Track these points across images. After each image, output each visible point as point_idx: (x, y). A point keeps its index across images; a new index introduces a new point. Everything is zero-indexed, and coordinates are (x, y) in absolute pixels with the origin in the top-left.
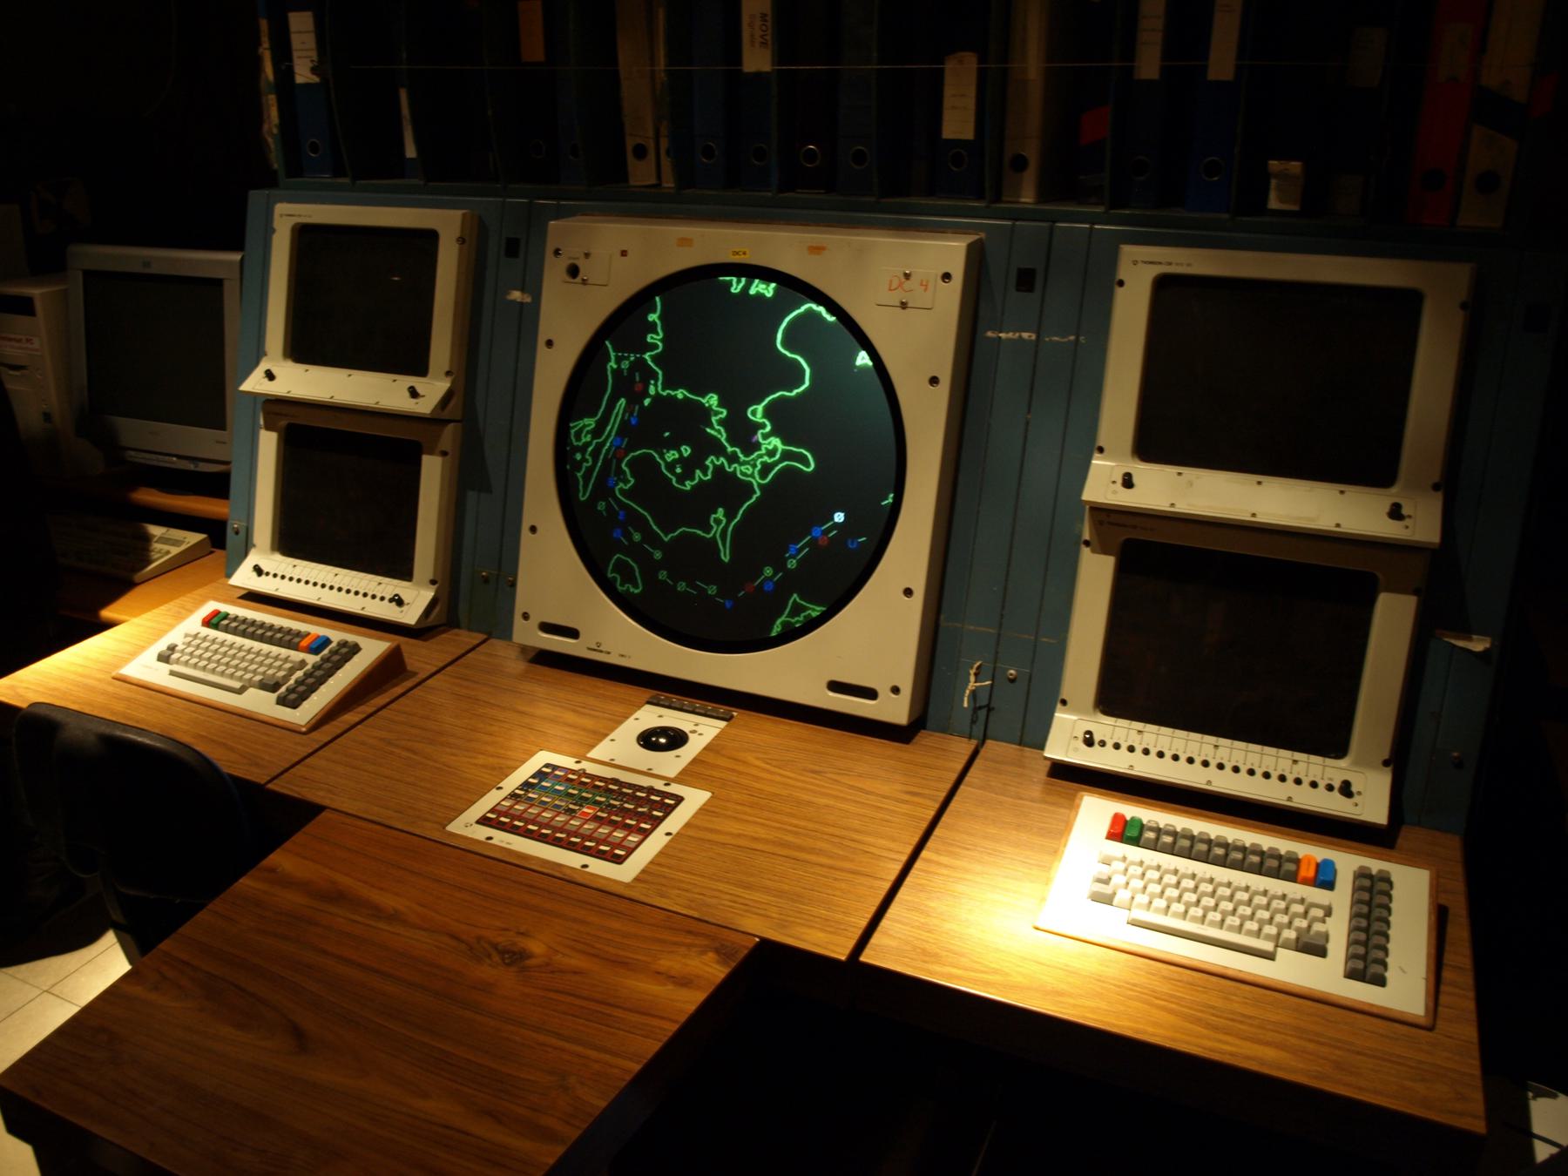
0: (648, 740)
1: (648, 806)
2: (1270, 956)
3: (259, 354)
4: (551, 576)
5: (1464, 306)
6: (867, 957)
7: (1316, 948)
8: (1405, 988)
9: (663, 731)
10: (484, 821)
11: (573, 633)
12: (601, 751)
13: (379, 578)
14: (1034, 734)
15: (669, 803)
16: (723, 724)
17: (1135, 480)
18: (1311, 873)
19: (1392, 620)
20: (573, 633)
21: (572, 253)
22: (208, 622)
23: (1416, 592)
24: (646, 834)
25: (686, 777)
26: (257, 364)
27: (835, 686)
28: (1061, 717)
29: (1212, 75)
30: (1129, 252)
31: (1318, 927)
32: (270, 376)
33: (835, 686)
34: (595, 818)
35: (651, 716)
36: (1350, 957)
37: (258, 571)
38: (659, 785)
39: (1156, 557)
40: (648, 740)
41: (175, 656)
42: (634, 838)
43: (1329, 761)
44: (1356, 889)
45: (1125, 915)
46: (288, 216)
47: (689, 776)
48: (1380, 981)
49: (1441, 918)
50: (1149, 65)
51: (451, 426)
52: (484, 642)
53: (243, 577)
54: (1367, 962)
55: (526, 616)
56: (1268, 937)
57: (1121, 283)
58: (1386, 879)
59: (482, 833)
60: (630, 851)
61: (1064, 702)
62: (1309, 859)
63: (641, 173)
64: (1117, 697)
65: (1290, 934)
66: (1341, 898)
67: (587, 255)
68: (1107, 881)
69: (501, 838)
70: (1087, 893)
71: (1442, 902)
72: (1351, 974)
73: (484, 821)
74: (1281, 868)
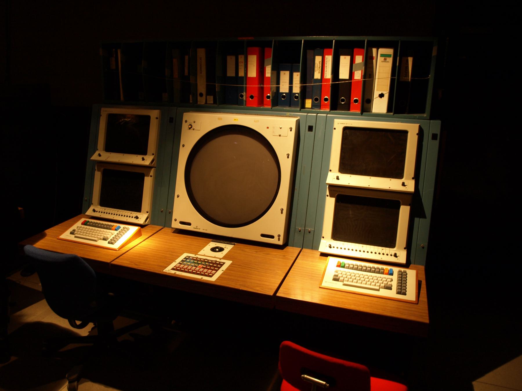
0: (213, 250)
1: (217, 265)
2: (378, 290)
3: (95, 149)
4: (183, 210)
6: (278, 294)
7: (389, 288)
8: (411, 295)
9: (217, 247)
10: (173, 269)
11: (189, 224)
12: (202, 252)
13: (131, 212)
14: (315, 246)
15: (222, 264)
16: (233, 246)
17: (339, 178)
18: (387, 272)
19: (404, 212)
20: (189, 224)
21: (190, 121)
22: (83, 224)
23: (409, 205)
24: (217, 271)
25: (225, 258)
26: (94, 152)
27: (263, 235)
28: (323, 241)
29: (299, 74)
30: (336, 121)
31: (389, 283)
32: (100, 155)
33: (263, 235)
34: (203, 268)
35: (213, 244)
36: (398, 289)
37: (94, 211)
38: (218, 260)
39: (344, 196)
40: (213, 250)
41: (76, 232)
42: (214, 272)
43: (391, 249)
44: (399, 274)
45: (342, 283)
46: (105, 112)
47: (226, 257)
48: (405, 294)
49: (419, 284)
50: (187, 58)
51: (153, 169)
52: (113, 261)
53: (89, 212)
54: (402, 290)
55: (176, 220)
56: (377, 286)
57: (157, 118)
58: (405, 272)
59: (173, 272)
60: (213, 275)
61: (323, 237)
62: (387, 269)
63: (201, 101)
64: (337, 235)
65: (383, 285)
66: (395, 277)
67: (194, 122)
68: (337, 276)
69: (178, 273)
70: (332, 279)
71: (419, 279)
72: (398, 293)
73: (173, 269)
74: (380, 271)
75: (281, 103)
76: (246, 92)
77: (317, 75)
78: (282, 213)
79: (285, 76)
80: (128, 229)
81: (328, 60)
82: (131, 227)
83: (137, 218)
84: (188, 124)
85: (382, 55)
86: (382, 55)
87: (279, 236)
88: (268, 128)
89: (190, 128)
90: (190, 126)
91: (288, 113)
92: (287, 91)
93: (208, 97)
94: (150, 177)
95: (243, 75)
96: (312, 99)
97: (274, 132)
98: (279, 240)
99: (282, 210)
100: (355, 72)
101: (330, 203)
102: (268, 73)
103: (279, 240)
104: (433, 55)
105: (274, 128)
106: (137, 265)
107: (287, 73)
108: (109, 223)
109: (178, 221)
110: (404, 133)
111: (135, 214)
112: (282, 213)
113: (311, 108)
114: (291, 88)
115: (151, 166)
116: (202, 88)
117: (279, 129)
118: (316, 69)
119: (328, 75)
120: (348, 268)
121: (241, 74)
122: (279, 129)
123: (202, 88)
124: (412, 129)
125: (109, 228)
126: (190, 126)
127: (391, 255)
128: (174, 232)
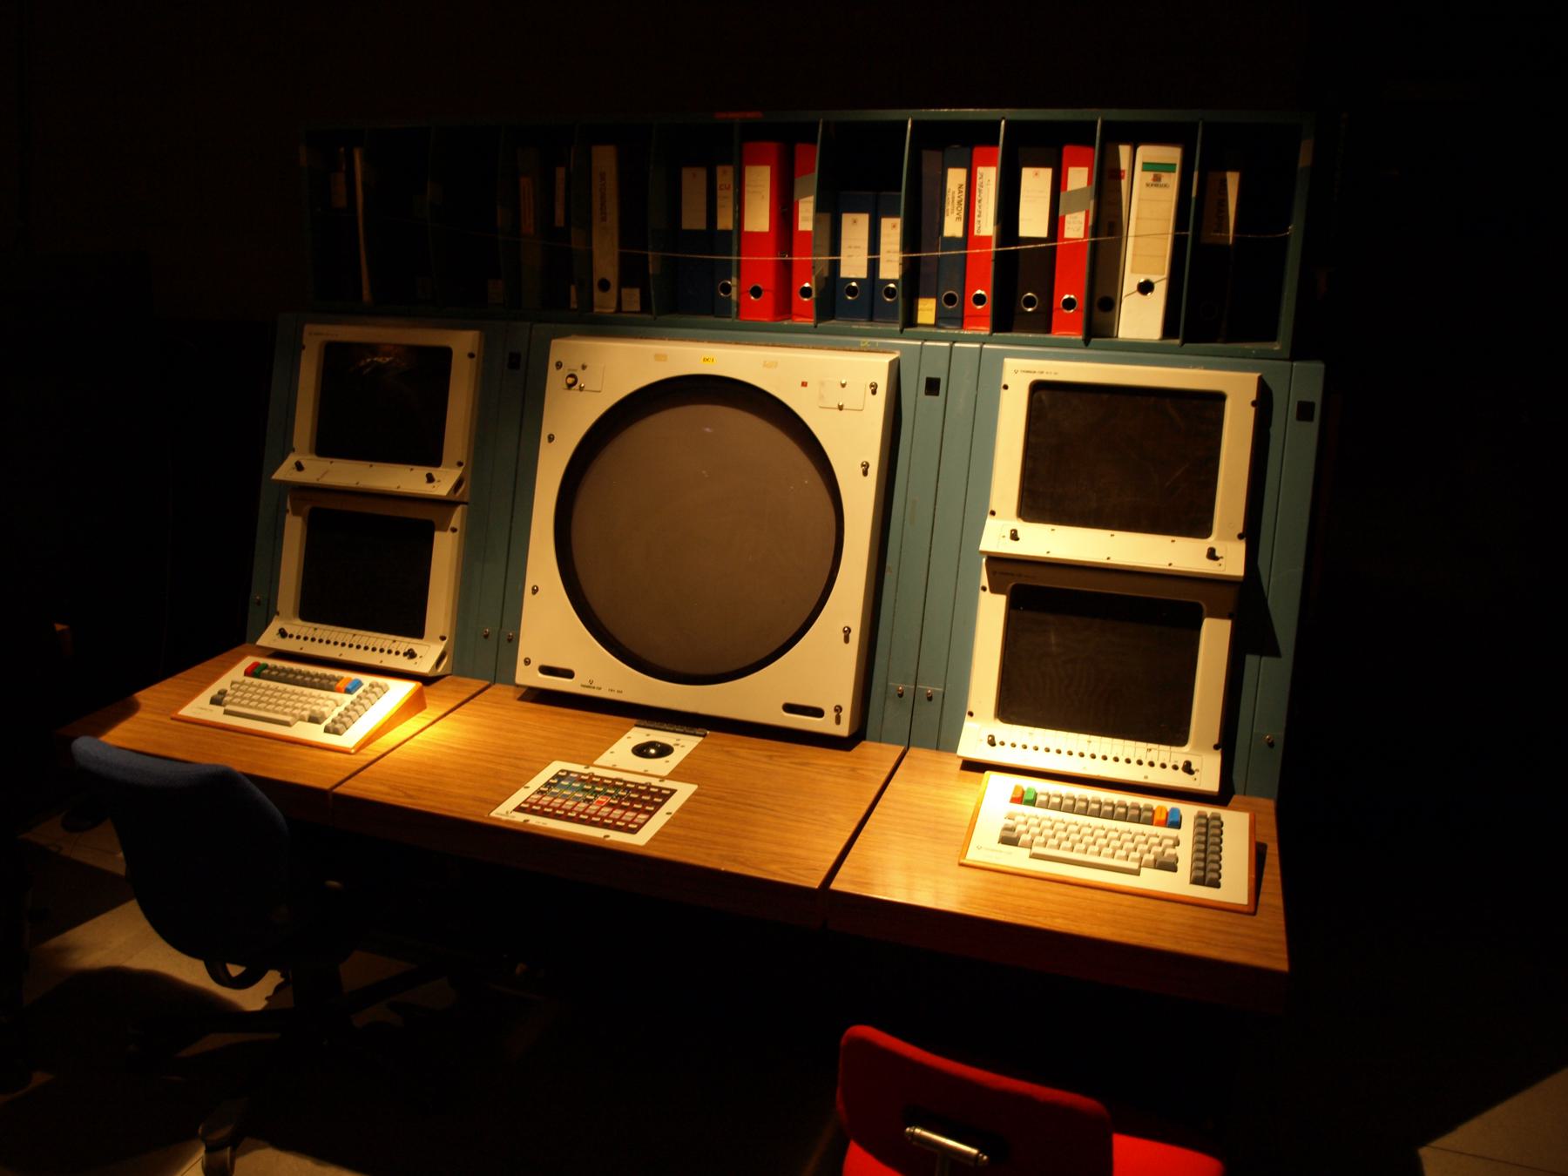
0: (641, 751)
1: (650, 799)
2: (1137, 873)
3: (286, 449)
4: (551, 632)
5: (1254, 404)
6: (835, 885)
7: (1170, 866)
8: (1234, 886)
9: (652, 744)
10: (519, 809)
11: (568, 674)
12: (606, 759)
13: (393, 637)
14: (945, 740)
15: (666, 796)
16: (700, 739)
17: (1019, 535)
18: (1163, 817)
19: (1215, 637)
20: (568, 674)
21: (571, 364)
22: (248, 673)
23: (1229, 617)
24: (651, 814)
25: (676, 775)
26: (284, 459)
27: (790, 708)
28: (969, 725)
30: (1010, 363)
31: (1170, 851)
32: (299, 467)
33: (790, 708)
34: (609, 805)
35: (639, 735)
36: (1194, 869)
37: (283, 633)
38: (655, 782)
39: (1033, 590)
40: (641, 751)
41: (227, 699)
42: (642, 817)
43: (1174, 749)
44: (1197, 825)
45: (1027, 852)
46: (316, 336)
47: (678, 774)
48: (1216, 884)
49: (1258, 855)
51: (459, 509)
52: (340, 784)
53: (269, 638)
54: (1207, 873)
55: (527, 662)
56: (1134, 860)
57: (471, 356)
58: (1218, 818)
59: (520, 817)
60: (641, 826)
61: (971, 714)
62: (1161, 809)
63: (605, 303)
64: (1012, 707)
65: (1151, 857)
66: (1187, 833)
67: (584, 367)
68: (1013, 829)
69: (535, 820)
70: (997, 838)
71: (1259, 839)
72: (1196, 881)
73: (519, 809)
74: (1141, 816)
75: (844, 309)
76: (739, 277)
77: (953, 227)
78: (847, 640)
79: (855, 228)
80: (384, 690)
81: (985, 180)
82: (393, 684)
83: (411, 654)
84: (564, 372)
85: (1147, 167)
86: (1147, 167)
87: (838, 709)
88: (804, 384)
89: (570, 386)
90: (570, 380)
91: (865, 341)
92: (863, 274)
93: (624, 291)
94: (449, 533)
95: (730, 227)
96: (937, 297)
97: (822, 397)
98: (838, 720)
99: (847, 632)
100: (1068, 218)
101: (992, 611)
102: (806, 219)
103: (838, 720)
104: (1300, 165)
105: (822, 384)
106: (410, 797)
107: (863, 220)
108: (329, 672)
109: (535, 664)
110: (1214, 401)
111: (404, 643)
112: (847, 640)
113: (936, 325)
114: (873, 266)
115: (453, 498)
116: (606, 264)
117: (837, 388)
118: (949, 207)
119: (986, 225)
120: (1046, 805)
121: (725, 222)
122: (837, 388)
123: (606, 264)
124: (1237, 387)
125: (327, 685)
126: (570, 380)
127: (1175, 768)
128: (522, 699)
